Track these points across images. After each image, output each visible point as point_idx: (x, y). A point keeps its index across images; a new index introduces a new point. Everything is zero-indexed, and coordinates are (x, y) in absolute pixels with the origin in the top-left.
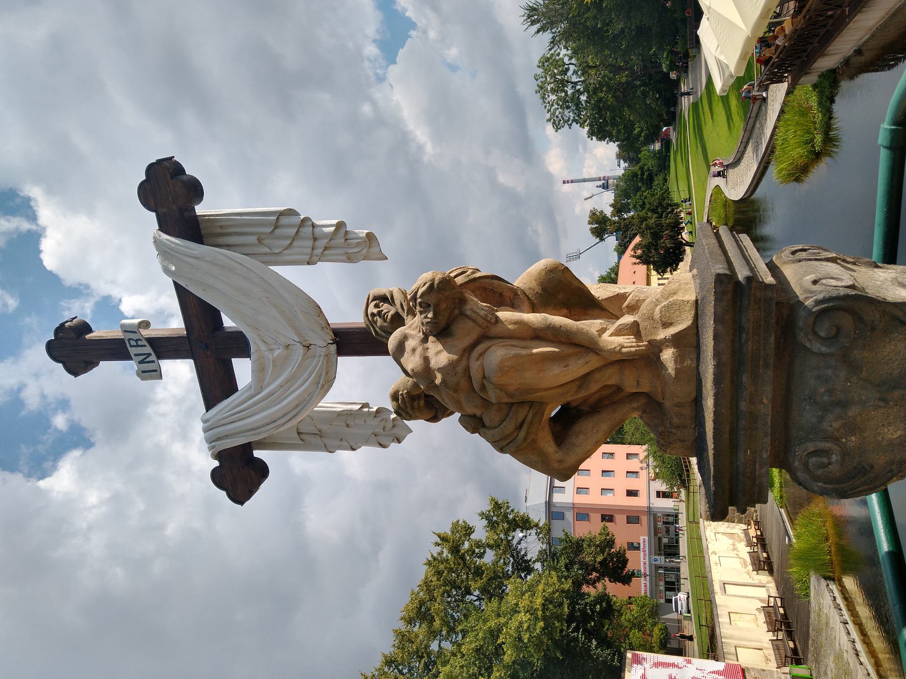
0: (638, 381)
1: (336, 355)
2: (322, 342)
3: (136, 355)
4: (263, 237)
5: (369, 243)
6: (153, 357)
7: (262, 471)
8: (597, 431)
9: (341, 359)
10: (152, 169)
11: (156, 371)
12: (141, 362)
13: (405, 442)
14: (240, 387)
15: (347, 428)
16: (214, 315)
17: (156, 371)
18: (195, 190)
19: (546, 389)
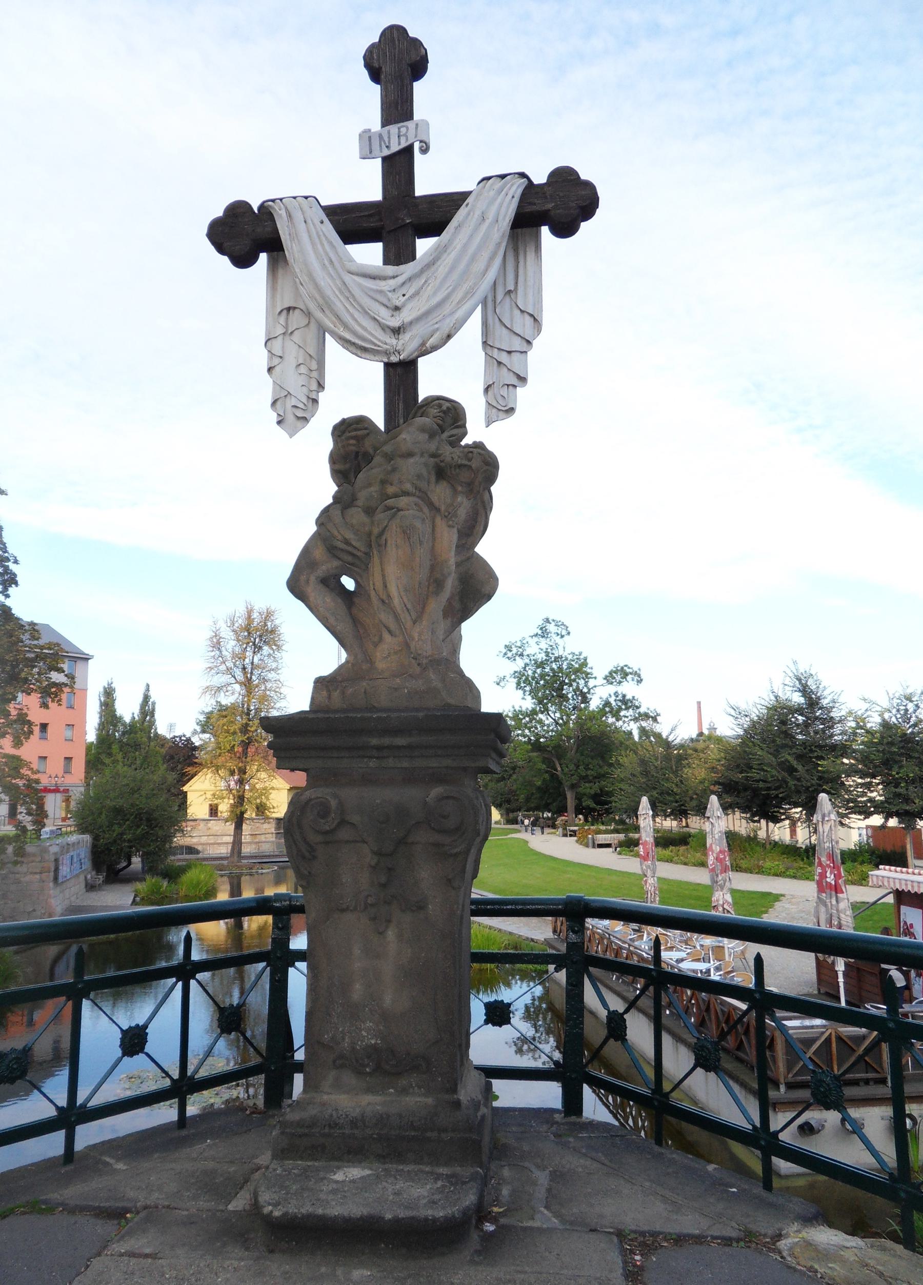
0: (433, 629)
1: (386, 360)
2: (406, 346)
3: (389, 132)
4: (513, 296)
5: (503, 409)
6: (386, 153)
7: (243, 260)
8: (337, 620)
9: (381, 366)
10: (589, 188)
11: (371, 152)
12: (380, 136)
13: (278, 427)
14: (346, 246)
15: (266, 369)
16: (435, 228)
17: (371, 152)
18: (565, 229)
19: (382, 570)
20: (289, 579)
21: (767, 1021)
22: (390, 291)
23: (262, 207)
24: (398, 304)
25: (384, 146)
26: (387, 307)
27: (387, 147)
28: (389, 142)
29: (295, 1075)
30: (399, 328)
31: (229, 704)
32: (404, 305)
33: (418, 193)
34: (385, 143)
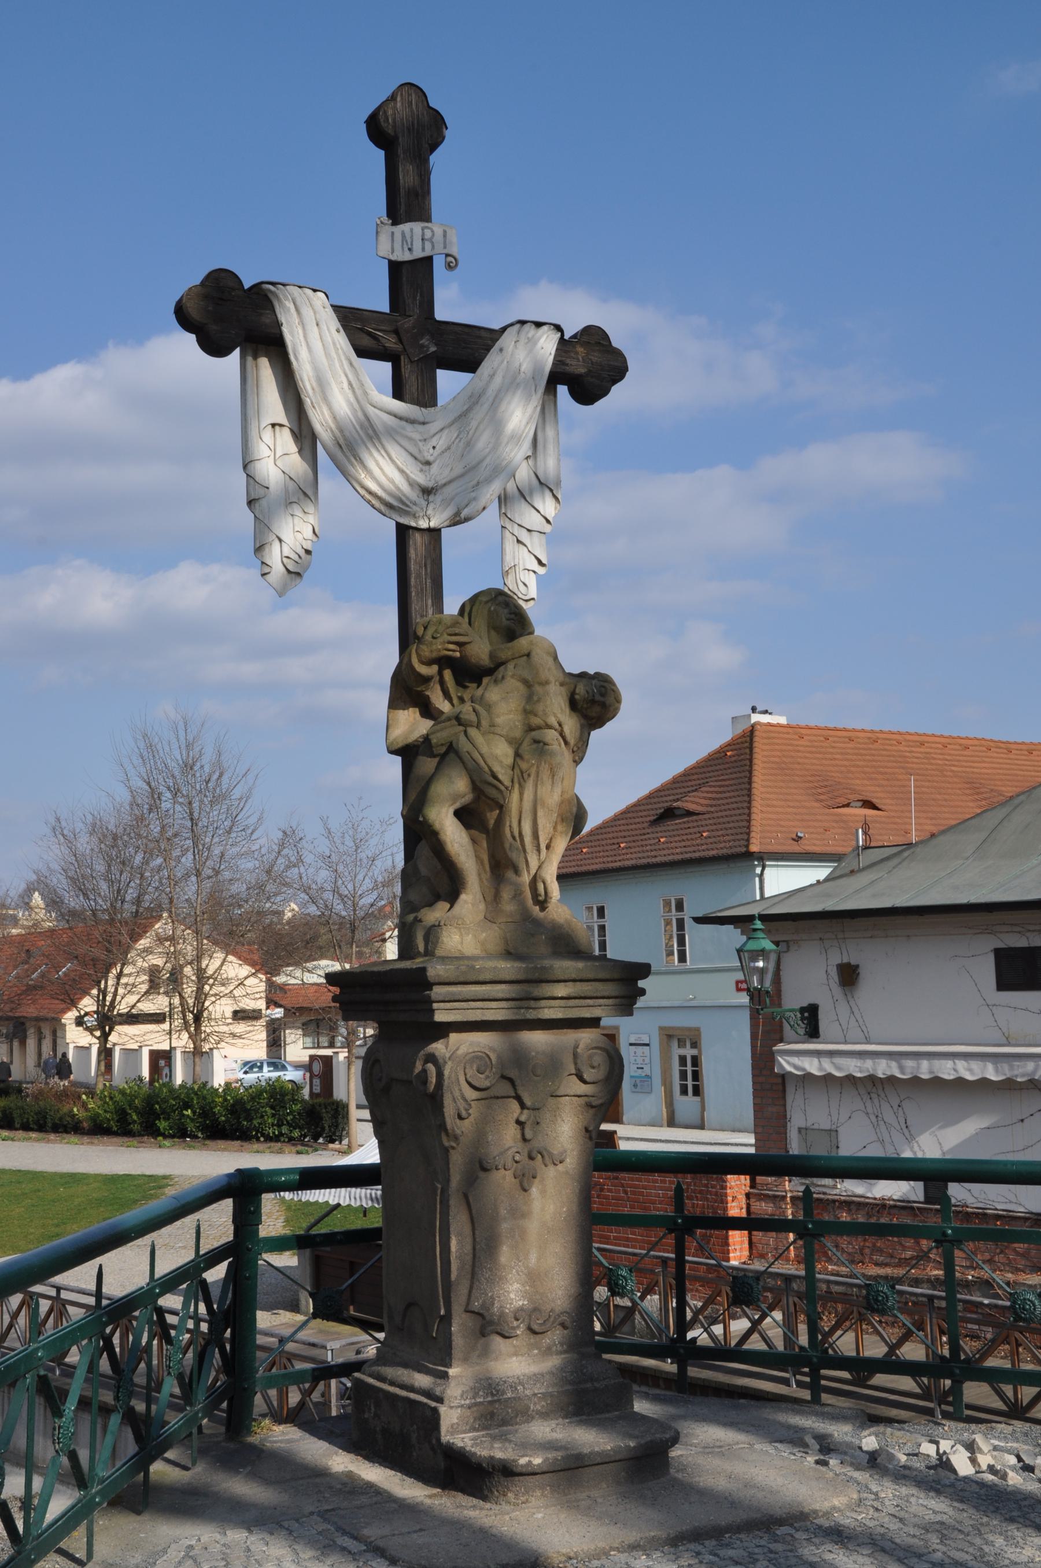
3: (412, 230)
20: (197, 341)
21: (941, 1272)
22: (420, 440)
23: (257, 286)
24: (431, 459)
25: (406, 249)
26: (416, 458)
27: (410, 249)
28: (412, 244)
29: (379, 1161)
30: (433, 488)
31: (264, 1083)
32: (434, 461)
33: (438, 371)
34: (407, 244)
